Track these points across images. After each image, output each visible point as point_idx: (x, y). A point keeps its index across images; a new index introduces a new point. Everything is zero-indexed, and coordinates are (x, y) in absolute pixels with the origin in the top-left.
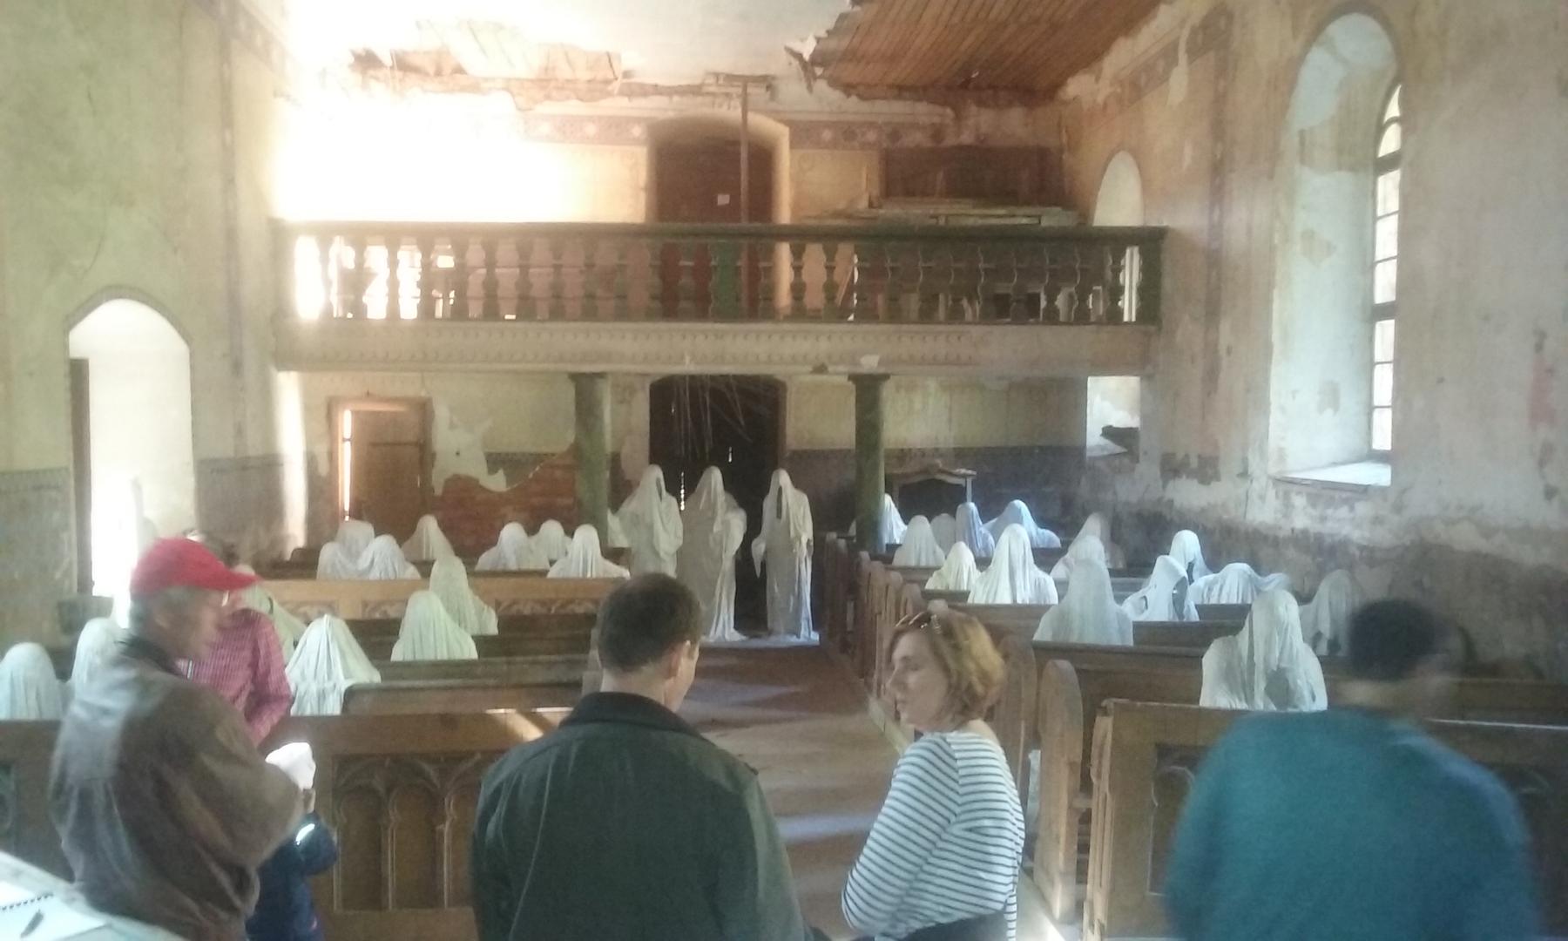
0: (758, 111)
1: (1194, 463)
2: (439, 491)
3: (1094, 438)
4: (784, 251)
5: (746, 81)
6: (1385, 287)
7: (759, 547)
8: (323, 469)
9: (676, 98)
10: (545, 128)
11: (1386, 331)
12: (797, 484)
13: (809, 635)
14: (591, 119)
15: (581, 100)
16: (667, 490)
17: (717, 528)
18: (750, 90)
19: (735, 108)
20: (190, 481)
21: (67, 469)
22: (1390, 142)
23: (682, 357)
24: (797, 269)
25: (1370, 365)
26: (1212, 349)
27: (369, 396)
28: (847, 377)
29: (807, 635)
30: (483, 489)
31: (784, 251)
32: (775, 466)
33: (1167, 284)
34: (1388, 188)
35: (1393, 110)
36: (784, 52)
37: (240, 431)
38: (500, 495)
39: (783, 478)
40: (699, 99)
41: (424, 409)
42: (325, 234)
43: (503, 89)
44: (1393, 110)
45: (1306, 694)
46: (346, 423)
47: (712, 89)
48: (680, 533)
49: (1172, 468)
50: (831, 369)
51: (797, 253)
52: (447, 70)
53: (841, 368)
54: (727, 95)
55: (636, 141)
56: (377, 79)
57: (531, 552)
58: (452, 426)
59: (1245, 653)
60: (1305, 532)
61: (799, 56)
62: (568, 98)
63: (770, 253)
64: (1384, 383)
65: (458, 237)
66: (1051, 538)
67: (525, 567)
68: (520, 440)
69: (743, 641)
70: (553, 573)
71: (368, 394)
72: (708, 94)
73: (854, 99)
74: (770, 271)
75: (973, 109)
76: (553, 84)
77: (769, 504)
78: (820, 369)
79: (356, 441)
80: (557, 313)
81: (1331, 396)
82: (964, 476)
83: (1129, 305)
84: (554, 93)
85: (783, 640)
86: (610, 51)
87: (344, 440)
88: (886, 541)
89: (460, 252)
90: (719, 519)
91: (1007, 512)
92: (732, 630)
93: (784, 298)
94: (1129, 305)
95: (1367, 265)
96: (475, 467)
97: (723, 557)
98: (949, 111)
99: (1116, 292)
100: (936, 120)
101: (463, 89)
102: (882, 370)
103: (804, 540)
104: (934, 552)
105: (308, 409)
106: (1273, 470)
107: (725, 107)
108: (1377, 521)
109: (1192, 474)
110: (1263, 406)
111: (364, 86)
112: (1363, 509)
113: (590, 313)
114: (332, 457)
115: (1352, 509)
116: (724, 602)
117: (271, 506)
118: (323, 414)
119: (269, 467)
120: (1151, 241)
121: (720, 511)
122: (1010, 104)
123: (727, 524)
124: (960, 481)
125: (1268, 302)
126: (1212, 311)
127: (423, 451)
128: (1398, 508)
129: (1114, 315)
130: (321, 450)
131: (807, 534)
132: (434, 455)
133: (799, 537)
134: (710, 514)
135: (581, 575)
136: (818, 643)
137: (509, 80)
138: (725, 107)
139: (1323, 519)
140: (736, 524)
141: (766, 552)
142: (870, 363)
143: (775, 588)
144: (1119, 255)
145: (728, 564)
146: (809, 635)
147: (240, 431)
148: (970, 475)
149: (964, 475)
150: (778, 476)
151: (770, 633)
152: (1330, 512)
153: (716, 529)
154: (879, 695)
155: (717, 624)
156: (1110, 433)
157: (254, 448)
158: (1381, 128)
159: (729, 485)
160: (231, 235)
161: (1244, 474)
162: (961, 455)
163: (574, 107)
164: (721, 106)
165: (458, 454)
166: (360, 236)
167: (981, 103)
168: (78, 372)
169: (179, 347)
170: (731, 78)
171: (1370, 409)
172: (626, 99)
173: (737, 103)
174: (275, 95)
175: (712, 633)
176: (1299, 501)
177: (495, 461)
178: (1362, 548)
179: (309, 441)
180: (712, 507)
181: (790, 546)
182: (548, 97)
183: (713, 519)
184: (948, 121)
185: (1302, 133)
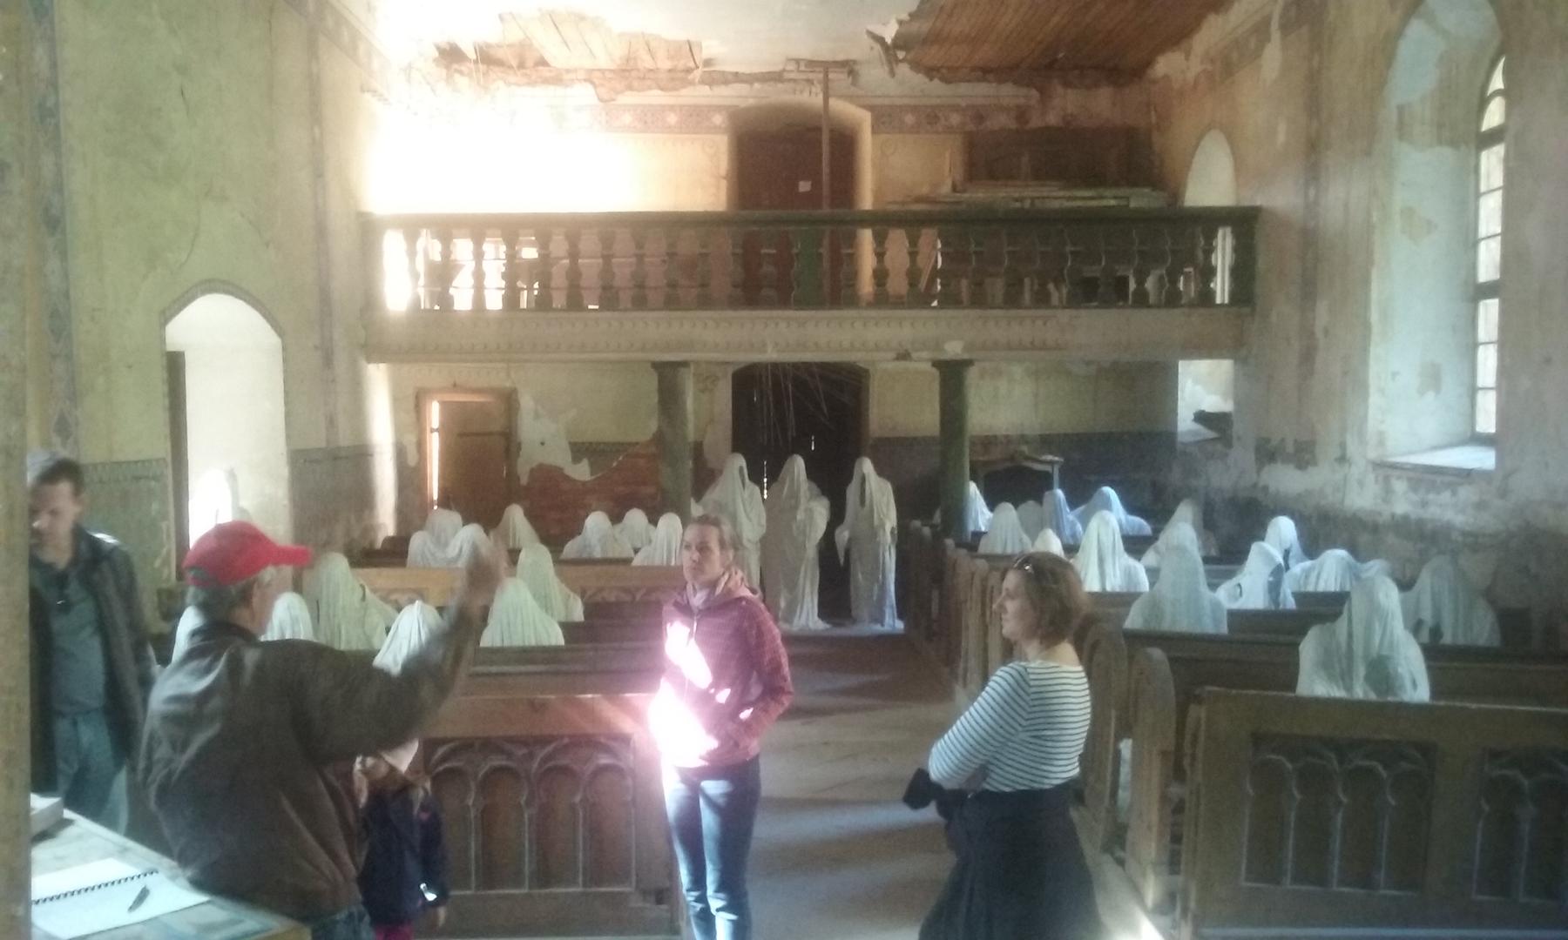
0: (840, 97)
1: (1290, 448)
2: (524, 480)
3: (1185, 422)
4: (866, 236)
5: (826, 66)
6: (1489, 261)
7: (843, 535)
8: (412, 460)
9: (757, 85)
10: (627, 118)
11: (1489, 312)
12: (880, 472)
13: (893, 624)
14: (672, 108)
15: (662, 89)
16: (750, 478)
17: (800, 516)
18: (831, 76)
19: (817, 94)
20: (284, 471)
21: (164, 459)
22: (1494, 115)
23: (764, 345)
24: (880, 255)
25: (1471, 347)
26: (1308, 333)
27: (455, 387)
28: (930, 364)
29: (891, 622)
30: (567, 478)
31: (866, 236)
32: (858, 454)
33: (1262, 264)
34: (1492, 163)
35: (1497, 82)
36: (866, 36)
37: (331, 422)
38: (584, 483)
39: (867, 466)
40: (780, 86)
41: (509, 400)
42: (412, 227)
43: (585, 80)
44: (1497, 82)
45: (1408, 684)
46: (434, 414)
47: (792, 76)
48: (764, 521)
49: (1267, 453)
50: (914, 355)
51: (880, 239)
52: (530, 63)
53: (925, 354)
54: (810, 82)
55: (714, 130)
56: (461, 73)
57: (616, 540)
58: (537, 416)
59: (1343, 638)
60: (1406, 518)
61: (880, 40)
62: (650, 88)
63: (852, 240)
64: (1488, 362)
65: (542, 227)
66: (1141, 525)
67: (610, 555)
68: (604, 430)
69: (827, 629)
70: (638, 561)
71: (455, 385)
72: (790, 80)
73: (936, 81)
74: (853, 259)
75: (1060, 90)
76: (634, 74)
77: (852, 492)
78: (904, 356)
79: (444, 430)
80: (640, 303)
81: (1432, 378)
82: (1051, 463)
83: (1221, 287)
84: (635, 84)
85: (866, 628)
86: (692, 39)
87: (432, 431)
88: (971, 528)
89: (543, 243)
90: (802, 507)
91: (1096, 498)
92: (816, 618)
93: (866, 285)
94: (1221, 287)
95: (1471, 243)
96: (559, 456)
97: (807, 546)
98: (1034, 93)
99: (1208, 273)
100: (1022, 101)
101: (546, 81)
102: (966, 356)
103: (888, 527)
104: (1021, 540)
105: (396, 401)
106: (1372, 454)
107: (806, 94)
108: (1481, 506)
109: (1287, 459)
110: (1362, 387)
111: (449, 79)
112: (1467, 493)
113: (672, 302)
114: (421, 446)
115: (1454, 493)
116: (808, 590)
117: (363, 497)
118: (411, 406)
119: (360, 457)
120: (1244, 221)
121: (803, 500)
122: (1096, 85)
123: (809, 512)
124: (1047, 468)
125: (1366, 282)
126: (1308, 291)
127: (509, 441)
128: (1503, 493)
129: (1206, 297)
130: (410, 440)
131: (890, 521)
132: (520, 444)
133: (883, 526)
134: (793, 502)
135: (665, 563)
136: (902, 632)
137: (591, 71)
138: (806, 94)
139: (1424, 504)
140: (820, 512)
141: (850, 540)
142: (954, 349)
143: (859, 577)
144: (1210, 236)
145: (811, 552)
146: (893, 624)
147: (331, 422)
148: (1057, 462)
149: (1051, 462)
150: (861, 464)
151: (855, 621)
152: (1431, 496)
153: (799, 517)
154: (965, 685)
155: (801, 612)
156: (1202, 418)
157: (344, 439)
158: (1483, 102)
159: (811, 475)
160: (321, 231)
161: (1343, 459)
162: (1047, 442)
163: (655, 97)
164: (801, 92)
165: (543, 444)
166: (446, 228)
167: (1067, 85)
168: (175, 365)
169: (271, 339)
170: (811, 64)
171: (1473, 390)
172: (707, 87)
173: (818, 89)
174: (363, 90)
175: (796, 621)
176: (1400, 486)
177: (580, 450)
178: (1465, 534)
179: (399, 430)
180: (795, 495)
181: (873, 533)
182: (630, 88)
183: (796, 508)
184: (1033, 102)
185: (1401, 109)
